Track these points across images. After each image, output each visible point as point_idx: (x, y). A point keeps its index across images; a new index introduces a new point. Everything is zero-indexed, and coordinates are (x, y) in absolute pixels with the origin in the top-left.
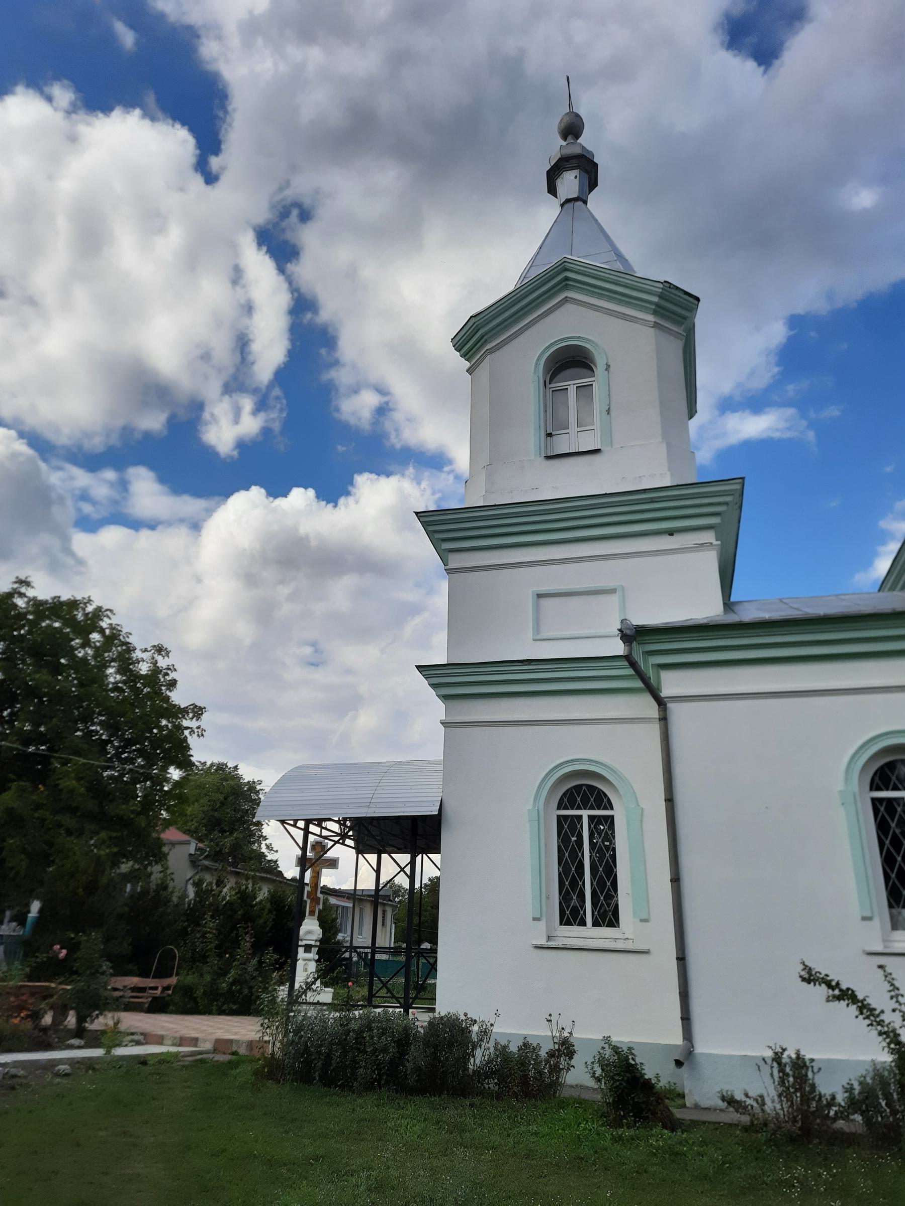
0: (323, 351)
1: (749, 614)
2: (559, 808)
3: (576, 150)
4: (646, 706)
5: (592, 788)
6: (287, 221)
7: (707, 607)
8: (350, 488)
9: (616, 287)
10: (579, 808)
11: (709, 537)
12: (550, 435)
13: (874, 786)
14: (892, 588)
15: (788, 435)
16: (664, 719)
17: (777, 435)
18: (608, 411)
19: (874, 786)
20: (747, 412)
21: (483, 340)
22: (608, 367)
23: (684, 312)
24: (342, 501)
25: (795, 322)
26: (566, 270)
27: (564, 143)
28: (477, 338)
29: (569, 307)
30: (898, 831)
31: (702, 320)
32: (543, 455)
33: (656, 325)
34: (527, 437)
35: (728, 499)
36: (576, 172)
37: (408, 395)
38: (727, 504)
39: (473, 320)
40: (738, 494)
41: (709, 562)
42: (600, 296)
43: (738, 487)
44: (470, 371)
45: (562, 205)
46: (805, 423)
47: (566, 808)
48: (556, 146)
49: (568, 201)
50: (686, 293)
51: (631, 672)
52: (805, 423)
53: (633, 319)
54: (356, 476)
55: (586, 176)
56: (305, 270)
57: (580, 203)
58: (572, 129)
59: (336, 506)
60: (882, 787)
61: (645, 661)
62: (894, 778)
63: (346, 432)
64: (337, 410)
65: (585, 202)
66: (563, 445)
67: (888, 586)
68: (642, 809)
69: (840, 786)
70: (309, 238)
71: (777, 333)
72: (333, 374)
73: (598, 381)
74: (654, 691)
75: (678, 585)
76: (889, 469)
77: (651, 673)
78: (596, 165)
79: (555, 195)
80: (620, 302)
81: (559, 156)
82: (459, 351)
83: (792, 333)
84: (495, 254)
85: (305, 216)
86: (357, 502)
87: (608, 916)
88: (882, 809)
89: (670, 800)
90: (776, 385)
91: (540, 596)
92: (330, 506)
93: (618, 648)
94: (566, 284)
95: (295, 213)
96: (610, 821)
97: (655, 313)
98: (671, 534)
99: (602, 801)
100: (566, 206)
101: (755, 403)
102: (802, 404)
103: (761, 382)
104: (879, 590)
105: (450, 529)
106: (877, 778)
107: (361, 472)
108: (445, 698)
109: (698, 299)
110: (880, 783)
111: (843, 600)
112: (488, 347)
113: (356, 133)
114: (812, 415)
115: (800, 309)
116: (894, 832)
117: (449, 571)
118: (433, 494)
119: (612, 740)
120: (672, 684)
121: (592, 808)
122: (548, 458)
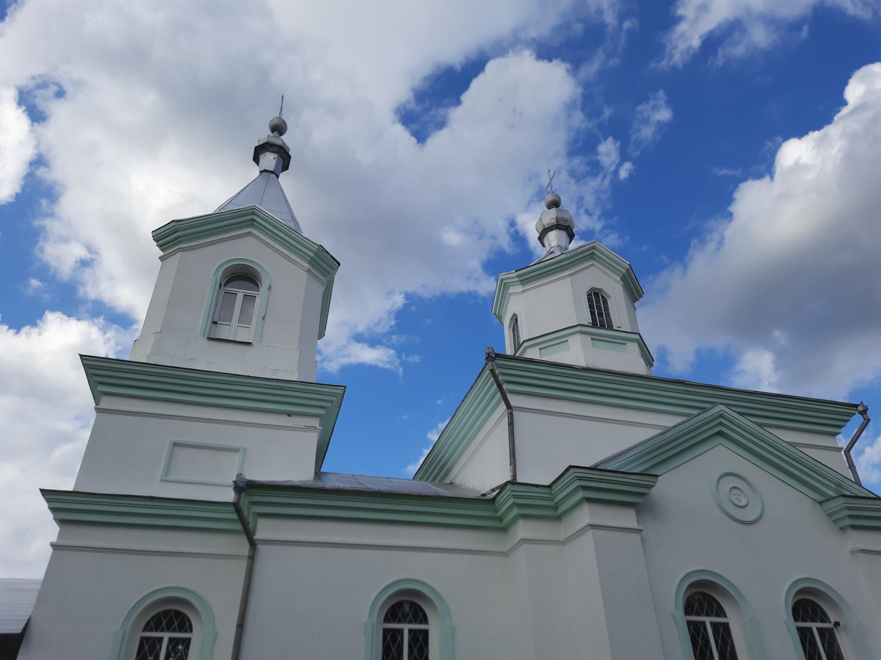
0: (44, 202)
1: (330, 483)
2: (145, 630)
3: (279, 143)
4: (241, 546)
5: (178, 614)
6: (42, 91)
7: (301, 472)
8: (38, 321)
9: (287, 237)
10: (400, 622)
11: (315, 422)
12: (215, 323)
13: (387, 620)
14: (421, 479)
15: (388, 366)
16: (252, 558)
17: (381, 365)
18: (264, 318)
19: (387, 620)
20: (366, 345)
21: (178, 240)
22: (270, 288)
23: (329, 270)
24: (26, 329)
25: (409, 297)
26: (254, 214)
27: (271, 135)
28: (173, 237)
29: (250, 239)
30: (395, 654)
31: (339, 276)
32: (206, 336)
33: (308, 271)
34: (200, 322)
35: (334, 399)
36: (276, 155)
37: (111, 259)
38: (332, 402)
39: (174, 224)
40: (340, 396)
41: (311, 441)
42: (275, 240)
43: (341, 392)
44: (162, 258)
45: (261, 172)
46: (399, 361)
47: (151, 630)
48: (264, 134)
49: (266, 171)
50: (332, 257)
51: (235, 516)
53: (295, 263)
54: (47, 312)
55: (281, 161)
56: (50, 133)
57: (274, 176)
58: (279, 128)
59: (18, 332)
61: (249, 509)
62: (400, 614)
63: (45, 273)
64: (42, 250)
65: (278, 176)
66: (224, 332)
68: (217, 633)
69: (365, 618)
70: (59, 111)
71: (399, 301)
72: (48, 222)
73: (261, 296)
74: (249, 534)
75: (283, 454)
77: (251, 520)
78: (290, 157)
79: (258, 164)
80: (288, 248)
81: (265, 141)
82: (157, 241)
84: (193, 182)
85: (60, 94)
86: (40, 334)
88: (389, 637)
89: (241, 626)
90: (389, 334)
91: (176, 444)
92: (12, 332)
93: (229, 496)
94: (252, 223)
95: (53, 89)
96: (426, 633)
97: (310, 263)
98: (290, 416)
99: (184, 624)
100: (264, 174)
101: (373, 342)
102: (400, 350)
103: (381, 329)
105: (101, 372)
107: (53, 309)
108: (61, 522)
109: (339, 264)
112: (182, 246)
113: (130, 58)
114: (404, 357)
115: (410, 290)
117: (98, 410)
118: (117, 344)
119: (206, 574)
120: (265, 530)
121: (174, 631)
122: (210, 339)
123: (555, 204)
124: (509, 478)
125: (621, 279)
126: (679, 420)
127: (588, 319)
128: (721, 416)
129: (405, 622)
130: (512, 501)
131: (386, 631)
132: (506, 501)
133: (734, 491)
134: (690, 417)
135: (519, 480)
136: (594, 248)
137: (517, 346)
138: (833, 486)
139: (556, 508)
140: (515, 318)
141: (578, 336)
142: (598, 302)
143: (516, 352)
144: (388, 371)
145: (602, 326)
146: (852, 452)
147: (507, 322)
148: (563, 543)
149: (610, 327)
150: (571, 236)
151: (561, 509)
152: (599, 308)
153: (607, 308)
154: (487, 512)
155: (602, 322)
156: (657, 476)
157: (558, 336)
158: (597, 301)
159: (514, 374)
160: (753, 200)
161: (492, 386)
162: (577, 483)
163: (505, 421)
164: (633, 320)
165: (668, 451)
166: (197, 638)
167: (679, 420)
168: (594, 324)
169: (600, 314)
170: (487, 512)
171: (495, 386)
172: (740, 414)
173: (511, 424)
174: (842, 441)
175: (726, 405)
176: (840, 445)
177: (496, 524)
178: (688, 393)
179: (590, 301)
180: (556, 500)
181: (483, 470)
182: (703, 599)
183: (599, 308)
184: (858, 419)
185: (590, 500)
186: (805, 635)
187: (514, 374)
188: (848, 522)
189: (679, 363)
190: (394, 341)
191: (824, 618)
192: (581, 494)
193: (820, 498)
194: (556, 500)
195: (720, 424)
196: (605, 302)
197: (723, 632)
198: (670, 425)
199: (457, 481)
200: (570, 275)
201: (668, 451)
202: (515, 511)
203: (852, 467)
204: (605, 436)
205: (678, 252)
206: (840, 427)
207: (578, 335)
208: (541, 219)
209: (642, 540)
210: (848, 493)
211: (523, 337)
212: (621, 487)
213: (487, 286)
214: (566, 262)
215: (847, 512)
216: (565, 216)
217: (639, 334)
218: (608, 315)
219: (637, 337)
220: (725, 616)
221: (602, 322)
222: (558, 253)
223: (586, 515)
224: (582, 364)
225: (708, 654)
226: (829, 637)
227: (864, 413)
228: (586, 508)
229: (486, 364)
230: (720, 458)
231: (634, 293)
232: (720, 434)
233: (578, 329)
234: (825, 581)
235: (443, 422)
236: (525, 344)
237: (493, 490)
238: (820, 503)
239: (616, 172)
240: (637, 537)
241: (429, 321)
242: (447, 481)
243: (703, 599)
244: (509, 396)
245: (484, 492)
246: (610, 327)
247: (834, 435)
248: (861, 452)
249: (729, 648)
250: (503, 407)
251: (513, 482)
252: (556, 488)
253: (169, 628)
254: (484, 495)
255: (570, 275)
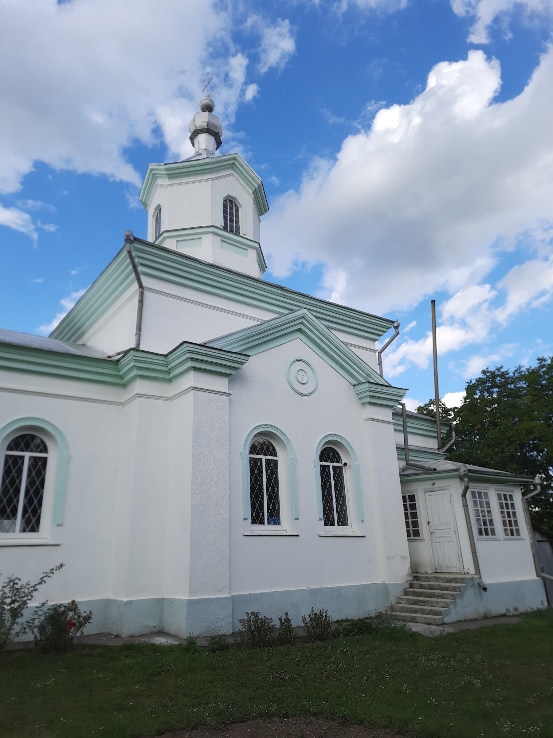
5: (33, 437)
10: (22, 450)
13: (10, 448)
14: (56, 338)
17: (14, 227)
30: (15, 475)
46: (33, 227)
52: (33, 227)
60: (24, 449)
62: (32, 445)
67: (54, 336)
76: (73, 272)
83: (33, 170)
87: (343, 521)
96: (45, 460)
104: (49, 337)
106: (12, 444)
110: (23, 447)
111: (25, 337)
114: (39, 224)
115: (46, 159)
116: (13, 475)
121: (31, 451)
123: (208, 108)
124: (133, 346)
125: (253, 193)
126: (274, 316)
127: (220, 222)
128: (303, 317)
129: (27, 451)
130: (133, 364)
131: (251, 459)
132: (128, 363)
133: (301, 372)
134: (282, 315)
135: (141, 348)
136: (235, 159)
137: (158, 235)
138: (365, 375)
139: (169, 372)
140: (159, 209)
141: (210, 235)
142: (231, 209)
143: (157, 239)
144: (21, 234)
145: (232, 231)
146: (382, 354)
147: (151, 211)
148: (170, 399)
149: (238, 233)
150: (219, 143)
151: (172, 374)
152: (231, 214)
153: (237, 216)
154: (111, 371)
155: (232, 227)
156: (249, 356)
157: (193, 233)
158: (230, 207)
159: (148, 258)
160: (353, 148)
161: (127, 267)
162: (188, 355)
163: (137, 298)
164: (257, 231)
165: (262, 338)
166: (281, 459)
167: (274, 316)
168: (225, 228)
169: (232, 221)
170: (111, 371)
171: (131, 267)
172: (317, 317)
173: (141, 301)
174: (378, 346)
175: (308, 309)
176: (377, 348)
177: (118, 381)
178: (285, 296)
179: (225, 206)
180: (170, 367)
181: (110, 337)
182: (264, 446)
183: (231, 214)
184: (392, 331)
185: (195, 369)
186: (324, 470)
187: (148, 258)
188: (368, 400)
189: (279, 271)
190: (29, 206)
191: (339, 460)
192: (190, 364)
193: (355, 382)
194: (170, 367)
195: (302, 323)
196: (237, 210)
197: (273, 466)
198: (267, 319)
199: (89, 344)
200: (212, 179)
201: (262, 338)
202: (135, 372)
203: (380, 364)
204: (217, 321)
205: (293, 177)
206: (380, 335)
207: (211, 235)
208: (194, 120)
209: (230, 401)
210: (372, 381)
211: (164, 228)
212: (220, 361)
213: (127, 173)
214: (209, 166)
215: (369, 394)
216: (215, 122)
217: (259, 244)
218: (237, 222)
219: (257, 245)
220: (276, 456)
221: (232, 227)
222: (204, 156)
223: (192, 379)
224: (211, 261)
225: (18, 481)
226: (339, 472)
227: (396, 327)
228: (192, 374)
229: (125, 246)
230: (296, 347)
231: (262, 206)
232: (299, 330)
233: (211, 229)
234: (289, 437)
235: (77, 291)
236: (165, 235)
237: (118, 354)
238: (354, 386)
239: (243, 91)
240: (227, 398)
241: (66, 193)
242: (80, 342)
243: (264, 446)
244: (142, 278)
245: (110, 354)
246: (238, 233)
247: (375, 340)
248: (387, 355)
249: (274, 476)
250: (136, 285)
251: (136, 349)
252: (171, 358)
253: (27, 448)
254: (110, 357)
255: (212, 179)
